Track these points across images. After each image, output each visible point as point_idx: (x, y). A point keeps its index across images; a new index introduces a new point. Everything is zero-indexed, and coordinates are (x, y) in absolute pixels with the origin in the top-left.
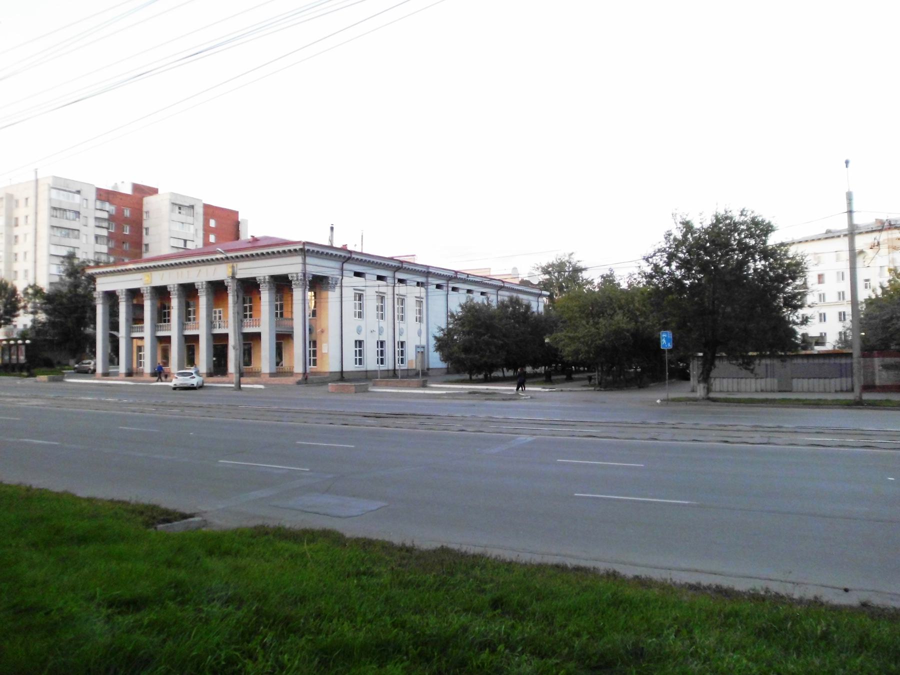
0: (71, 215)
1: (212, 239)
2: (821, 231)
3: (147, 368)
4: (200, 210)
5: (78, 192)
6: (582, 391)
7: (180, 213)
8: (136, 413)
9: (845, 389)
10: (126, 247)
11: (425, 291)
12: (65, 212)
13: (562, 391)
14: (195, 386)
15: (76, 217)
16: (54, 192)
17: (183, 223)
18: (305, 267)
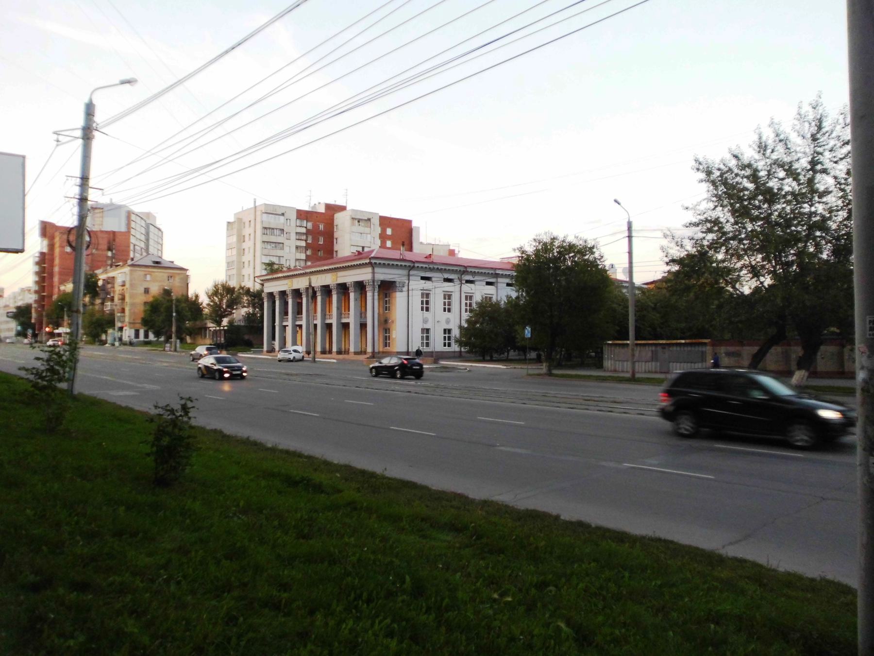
0: (277, 232)
1: (389, 244)
3: (319, 349)
4: (376, 221)
5: (283, 214)
6: (538, 368)
7: (795, 119)
8: (347, 387)
9: (610, 370)
10: (320, 254)
11: (496, 288)
12: (273, 230)
13: (515, 368)
14: (292, 359)
15: (281, 233)
16: (265, 215)
17: (361, 233)
18: (374, 275)
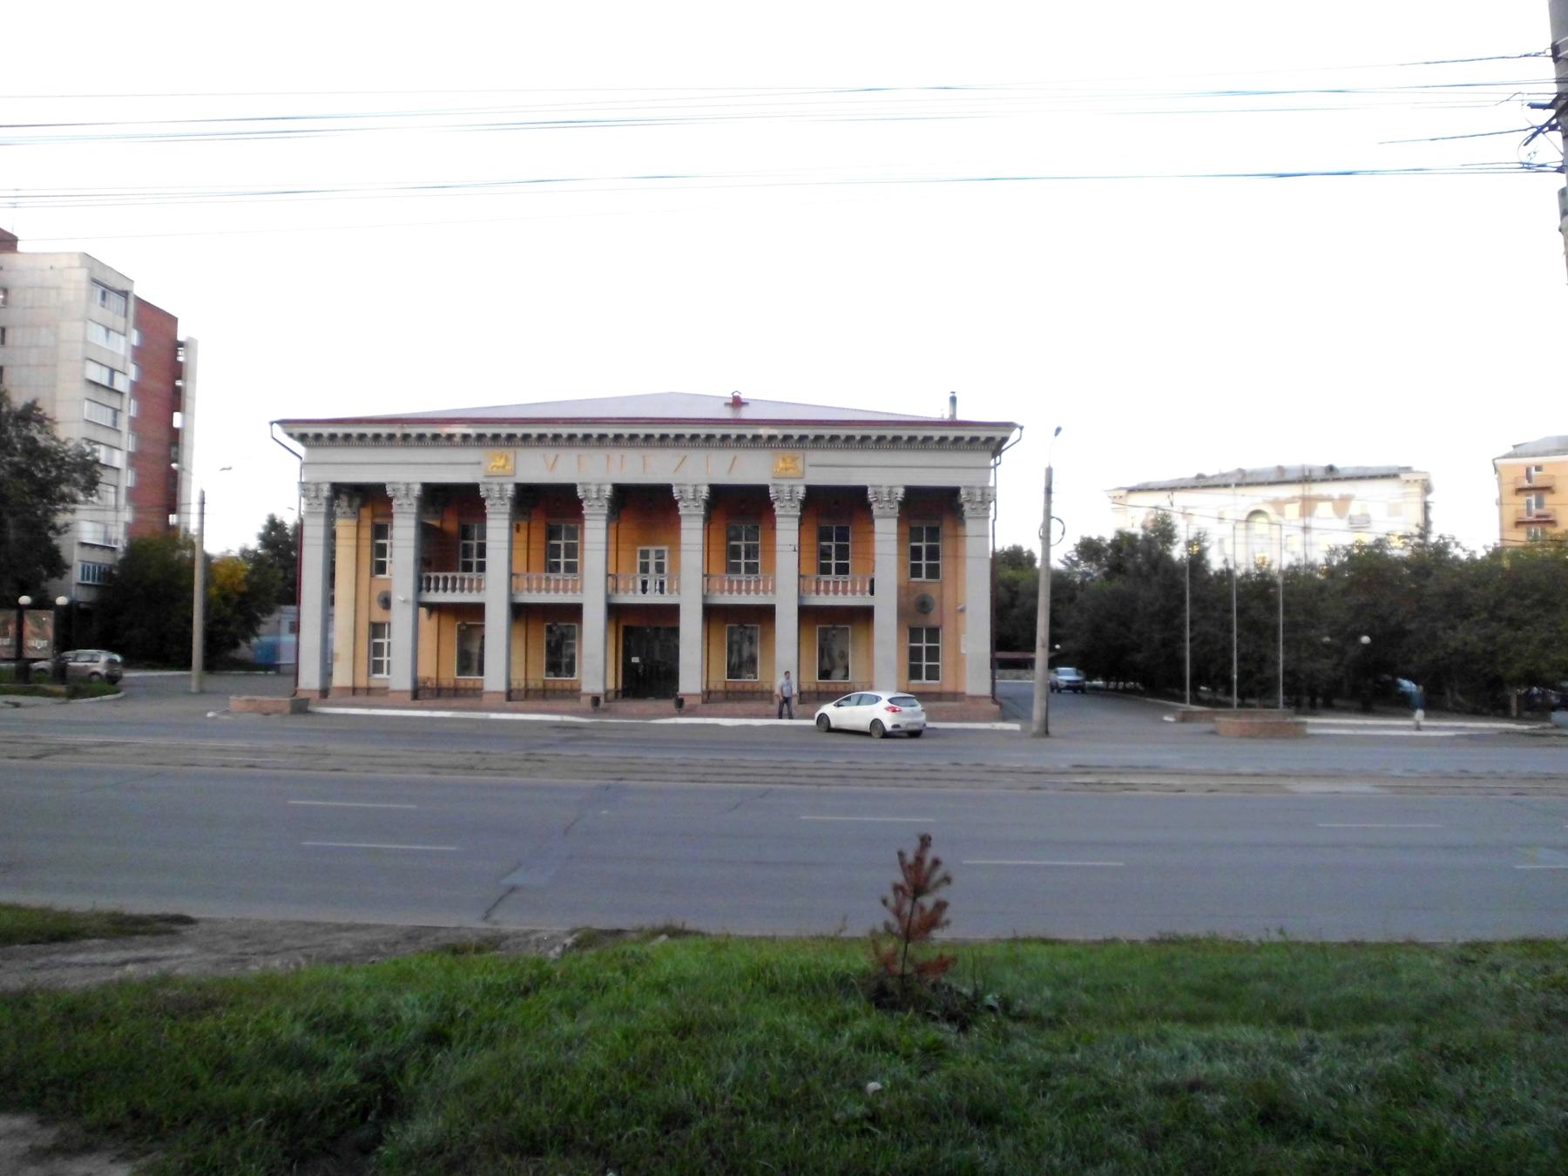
2: (1189, 474)
